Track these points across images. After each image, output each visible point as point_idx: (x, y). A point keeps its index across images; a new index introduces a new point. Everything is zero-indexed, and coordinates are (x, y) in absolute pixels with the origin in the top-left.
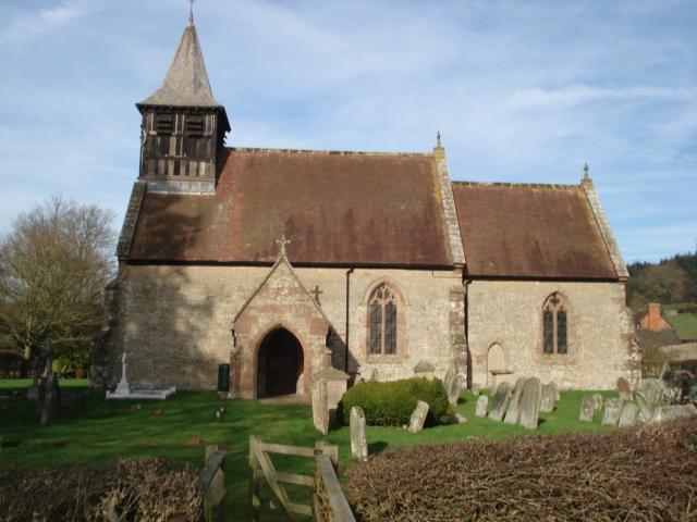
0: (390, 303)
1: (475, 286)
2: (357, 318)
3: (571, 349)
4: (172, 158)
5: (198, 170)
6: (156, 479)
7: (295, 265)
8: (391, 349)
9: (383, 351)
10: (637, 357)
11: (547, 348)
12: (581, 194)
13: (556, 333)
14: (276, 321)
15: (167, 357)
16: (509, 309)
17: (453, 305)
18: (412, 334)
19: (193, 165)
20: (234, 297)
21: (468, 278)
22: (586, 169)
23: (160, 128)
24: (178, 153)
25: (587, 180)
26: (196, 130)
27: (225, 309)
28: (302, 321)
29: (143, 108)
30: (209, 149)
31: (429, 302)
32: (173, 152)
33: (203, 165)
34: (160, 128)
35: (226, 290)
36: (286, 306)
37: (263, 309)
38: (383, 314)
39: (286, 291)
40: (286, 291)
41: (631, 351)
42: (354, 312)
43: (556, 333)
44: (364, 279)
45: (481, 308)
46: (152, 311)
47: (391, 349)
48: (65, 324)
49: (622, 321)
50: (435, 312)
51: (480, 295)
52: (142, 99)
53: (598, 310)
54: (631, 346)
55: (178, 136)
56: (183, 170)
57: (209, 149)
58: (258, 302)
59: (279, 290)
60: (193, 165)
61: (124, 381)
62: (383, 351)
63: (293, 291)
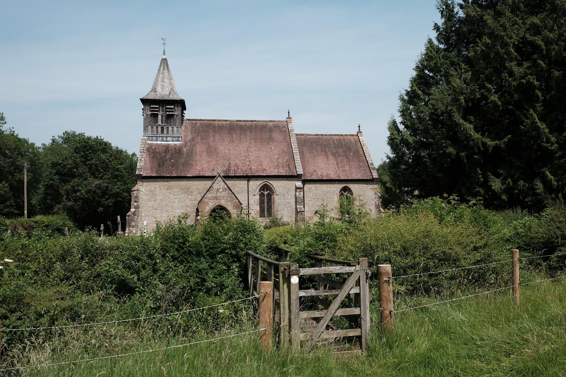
1: (307, 186)
2: (253, 201)
4: (160, 125)
14: (218, 204)
18: (279, 208)
20: (195, 192)
22: (359, 127)
24: (162, 123)
27: (191, 199)
28: (229, 203)
31: (287, 193)
32: (160, 123)
36: (221, 197)
38: (25, 173)
39: (221, 190)
40: (221, 190)
42: (188, 191)
44: (255, 185)
45: (311, 195)
48: (492, 35)
50: (289, 197)
51: (310, 189)
52: (143, 96)
56: (165, 131)
58: (209, 195)
59: (218, 190)
60: (170, 129)
63: (224, 190)
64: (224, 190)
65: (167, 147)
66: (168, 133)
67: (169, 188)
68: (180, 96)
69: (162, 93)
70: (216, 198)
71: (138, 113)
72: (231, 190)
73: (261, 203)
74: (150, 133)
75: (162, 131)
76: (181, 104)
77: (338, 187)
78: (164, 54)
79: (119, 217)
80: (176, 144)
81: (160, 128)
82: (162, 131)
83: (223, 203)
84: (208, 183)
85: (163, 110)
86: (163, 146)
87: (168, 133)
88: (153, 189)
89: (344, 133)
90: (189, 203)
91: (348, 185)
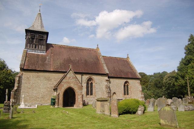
0: (92, 82)
1: (111, 80)
3: (130, 94)
5: (41, 47)
6: (140, 100)
7: (76, 73)
8: (92, 94)
9: (90, 95)
10: (143, 95)
11: (125, 94)
12: (127, 60)
13: (126, 91)
14: (69, 86)
15: (33, 97)
16: (118, 84)
17: (107, 83)
19: (40, 46)
21: (109, 77)
23: (31, 36)
24: (36, 43)
25: (128, 57)
26: (33, 36)
28: (76, 86)
29: (27, 31)
30: (44, 43)
32: (34, 43)
33: (43, 46)
34: (31, 36)
35: (50, 78)
37: (65, 83)
39: (71, 78)
40: (71, 78)
41: (142, 94)
42: (49, 79)
43: (126, 91)
44: (85, 77)
46: (30, 84)
47: (92, 94)
49: (140, 88)
52: (27, 28)
53: (135, 86)
54: (142, 93)
55: (36, 39)
56: (37, 47)
57: (44, 43)
60: (40, 46)
61: (23, 103)
62: (90, 95)
63: (73, 78)
64: (73, 78)
65: (38, 55)
66: (38, 48)
67: (38, 77)
68: (45, 30)
69: (38, 28)
70: (68, 83)
71: (22, 41)
72: (77, 79)
73: (87, 88)
74: (28, 47)
75: (35, 48)
76: (47, 34)
77: (123, 81)
78: (40, 11)
79: (7, 90)
80: (43, 54)
81: (34, 46)
82: (35, 48)
83: (72, 85)
84: (61, 75)
85: (36, 37)
86: (36, 54)
87: (38, 48)
88: (28, 77)
89: (121, 57)
90: (49, 86)
91: (128, 80)
